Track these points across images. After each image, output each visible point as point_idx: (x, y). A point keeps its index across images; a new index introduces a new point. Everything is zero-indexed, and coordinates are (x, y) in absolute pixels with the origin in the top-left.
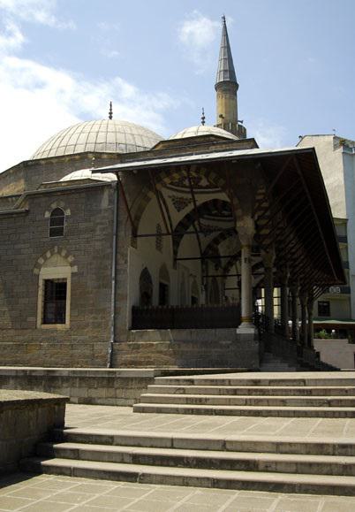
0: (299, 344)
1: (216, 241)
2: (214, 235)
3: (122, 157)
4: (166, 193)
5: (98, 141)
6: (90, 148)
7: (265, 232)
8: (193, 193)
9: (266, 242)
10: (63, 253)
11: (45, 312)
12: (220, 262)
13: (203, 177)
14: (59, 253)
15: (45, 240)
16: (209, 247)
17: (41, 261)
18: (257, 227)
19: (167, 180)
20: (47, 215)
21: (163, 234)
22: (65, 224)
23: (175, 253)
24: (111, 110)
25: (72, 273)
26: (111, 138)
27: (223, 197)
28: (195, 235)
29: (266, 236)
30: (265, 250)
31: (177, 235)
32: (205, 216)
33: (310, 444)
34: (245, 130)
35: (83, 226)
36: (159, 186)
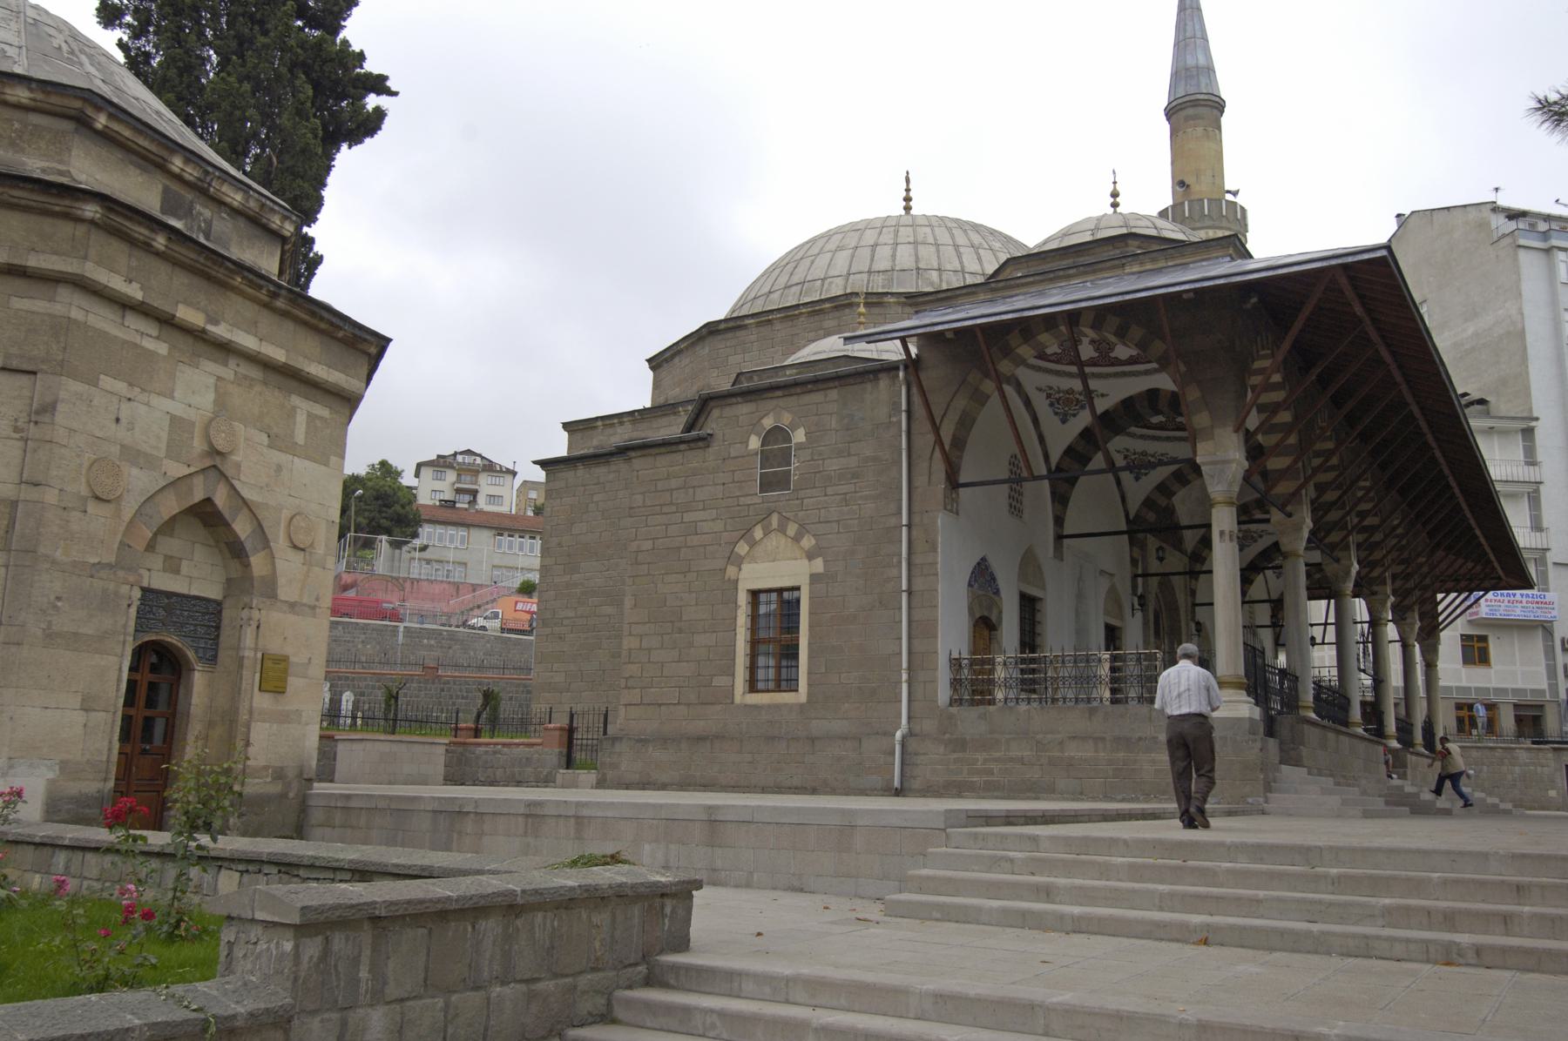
0: (1394, 744)
1: (1163, 489)
2: (1161, 473)
3: (916, 301)
4: (1031, 380)
5: (876, 267)
6: (859, 284)
7: (1275, 463)
8: (1084, 378)
9: (1284, 488)
10: (792, 529)
11: (753, 668)
12: (1181, 540)
13: (1113, 339)
14: (782, 529)
15: (748, 500)
16: (1148, 503)
17: (742, 548)
18: (1255, 452)
19: (1025, 351)
20: (754, 443)
21: (1025, 480)
22: (795, 463)
23: (1059, 521)
24: (908, 190)
25: (812, 576)
26: (905, 258)
27: (1164, 382)
28: (1110, 476)
29: (1283, 474)
30: (1282, 509)
31: (1063, 480)
32: (1133, 429)
33: (826, 793)
34: (1243, 210)
35: (833, 465)
36: (1005, 366)
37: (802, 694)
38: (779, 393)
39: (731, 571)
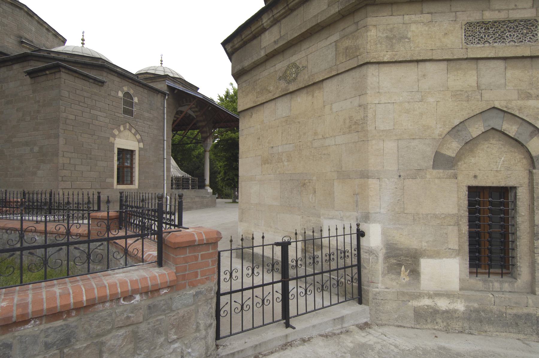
37: (136, 185)
38: (130, 81)
39: (112, 139)
